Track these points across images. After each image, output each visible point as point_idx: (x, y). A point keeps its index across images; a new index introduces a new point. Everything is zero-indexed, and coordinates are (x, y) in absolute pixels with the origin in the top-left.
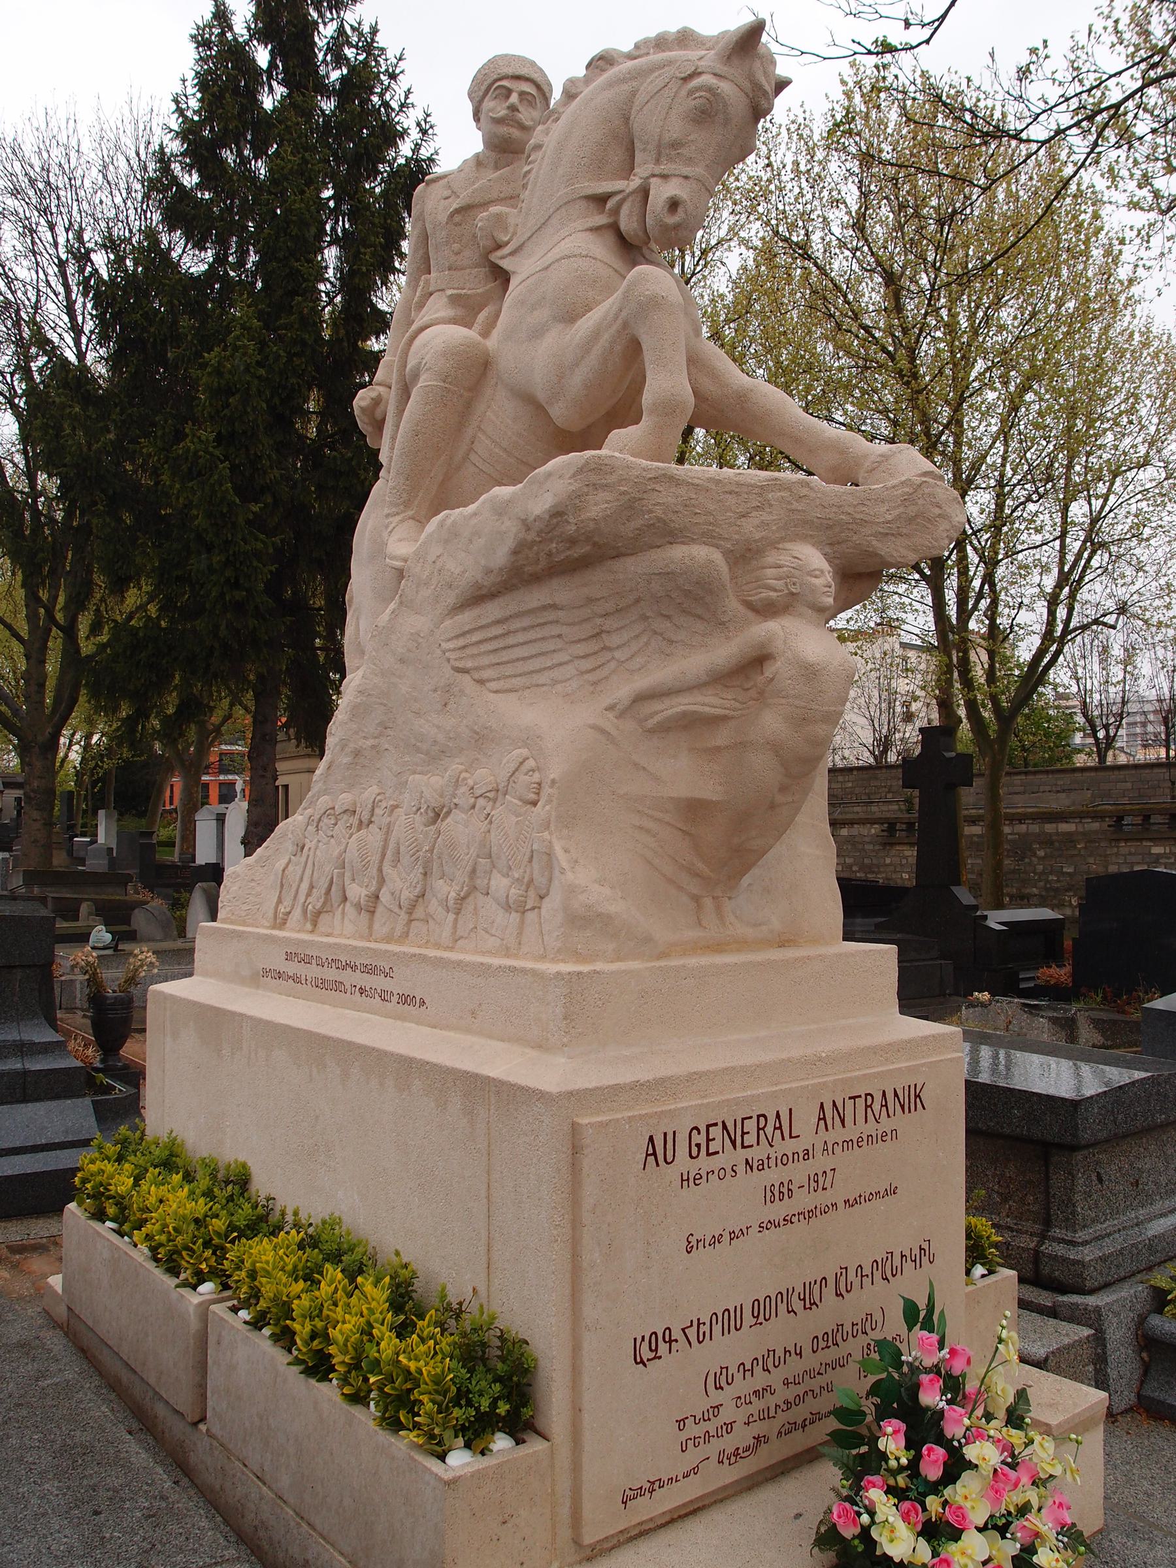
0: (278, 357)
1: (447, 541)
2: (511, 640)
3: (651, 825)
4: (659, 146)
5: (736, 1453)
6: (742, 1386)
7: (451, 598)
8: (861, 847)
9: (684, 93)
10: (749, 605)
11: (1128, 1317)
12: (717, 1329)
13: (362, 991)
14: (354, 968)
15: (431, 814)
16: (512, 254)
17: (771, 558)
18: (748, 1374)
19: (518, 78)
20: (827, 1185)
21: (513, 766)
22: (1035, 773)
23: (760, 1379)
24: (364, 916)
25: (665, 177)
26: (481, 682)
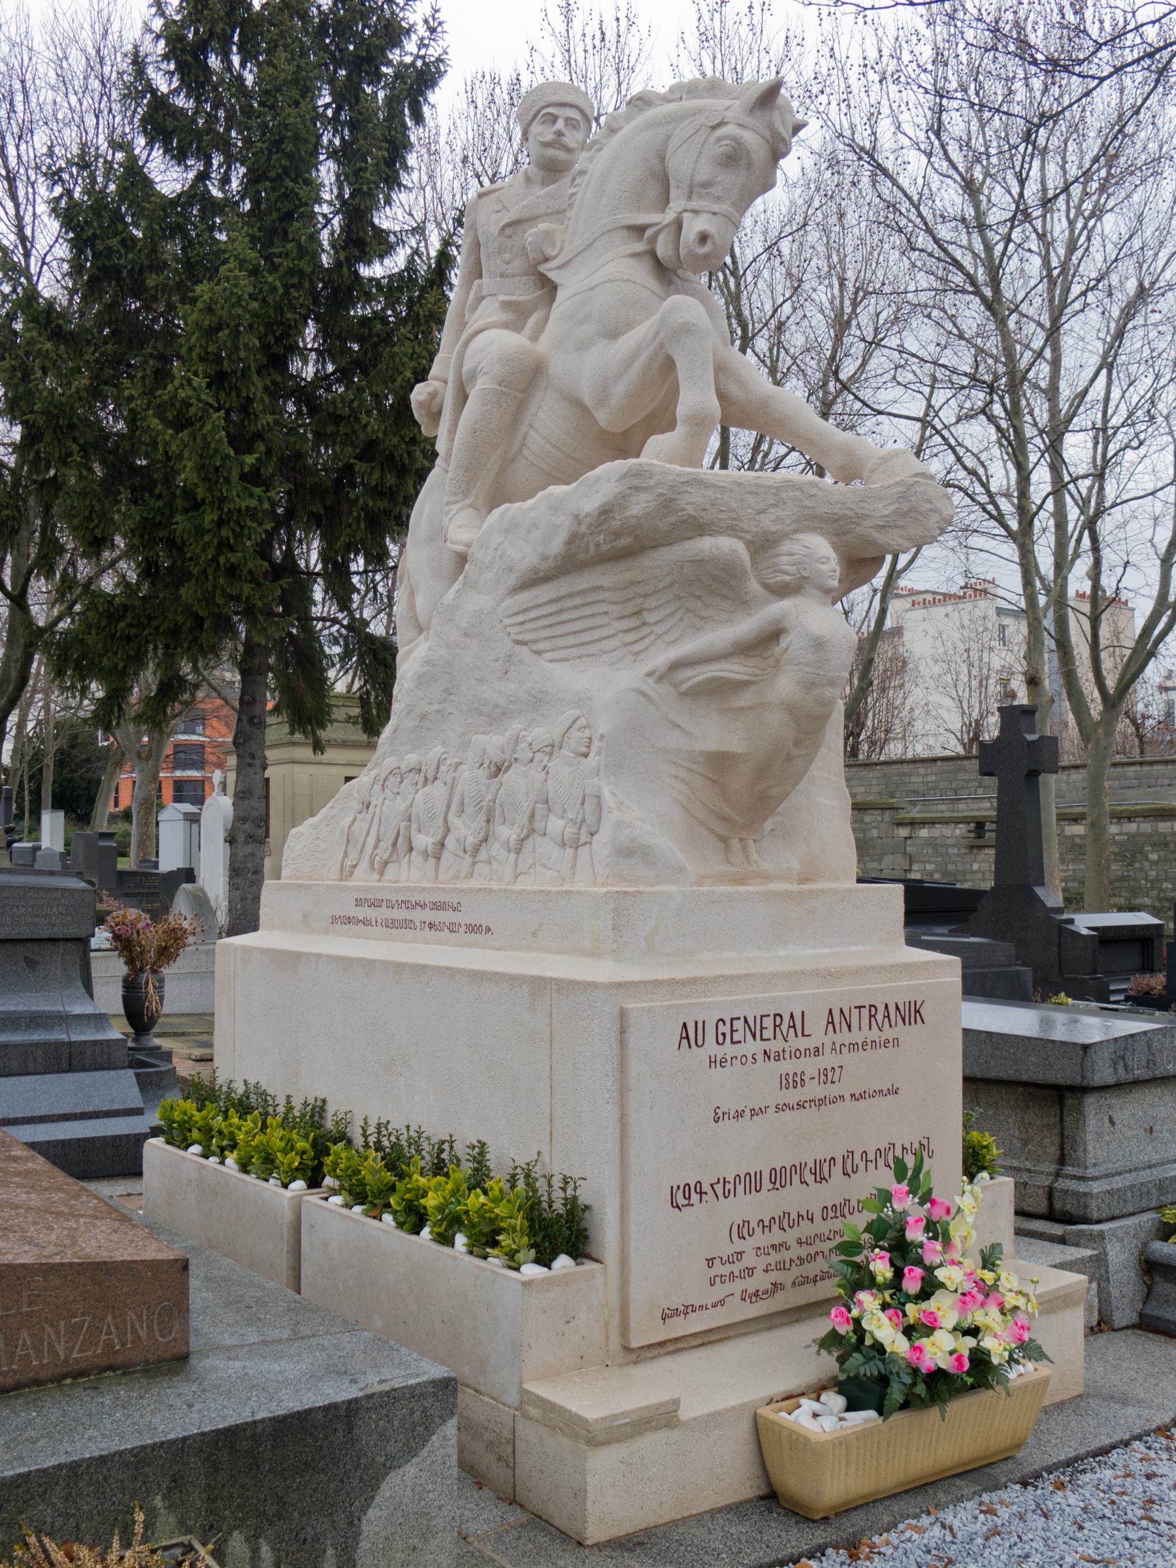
0: (275, 288)
1: (507, 531)
2: (564, 617)
4: (691, 186)
5: (756, 1294)
6: (762, 1239)
7: (512, 580)
8: (943, 850)
9: (712, 139)
11: (1132, 1244)
12: (740, 1188)
13: (431, 926)
14: (423, 906)
15: (493, 768)
16: (559, 268)
17: (786, 546)
19: (563, 105)
20: (836, 1079)
21: (567, 724)
22: (1152, 763)
23: (776, 1236)
24: (431, 862)
25: (695, 212)
26: (538, 653)
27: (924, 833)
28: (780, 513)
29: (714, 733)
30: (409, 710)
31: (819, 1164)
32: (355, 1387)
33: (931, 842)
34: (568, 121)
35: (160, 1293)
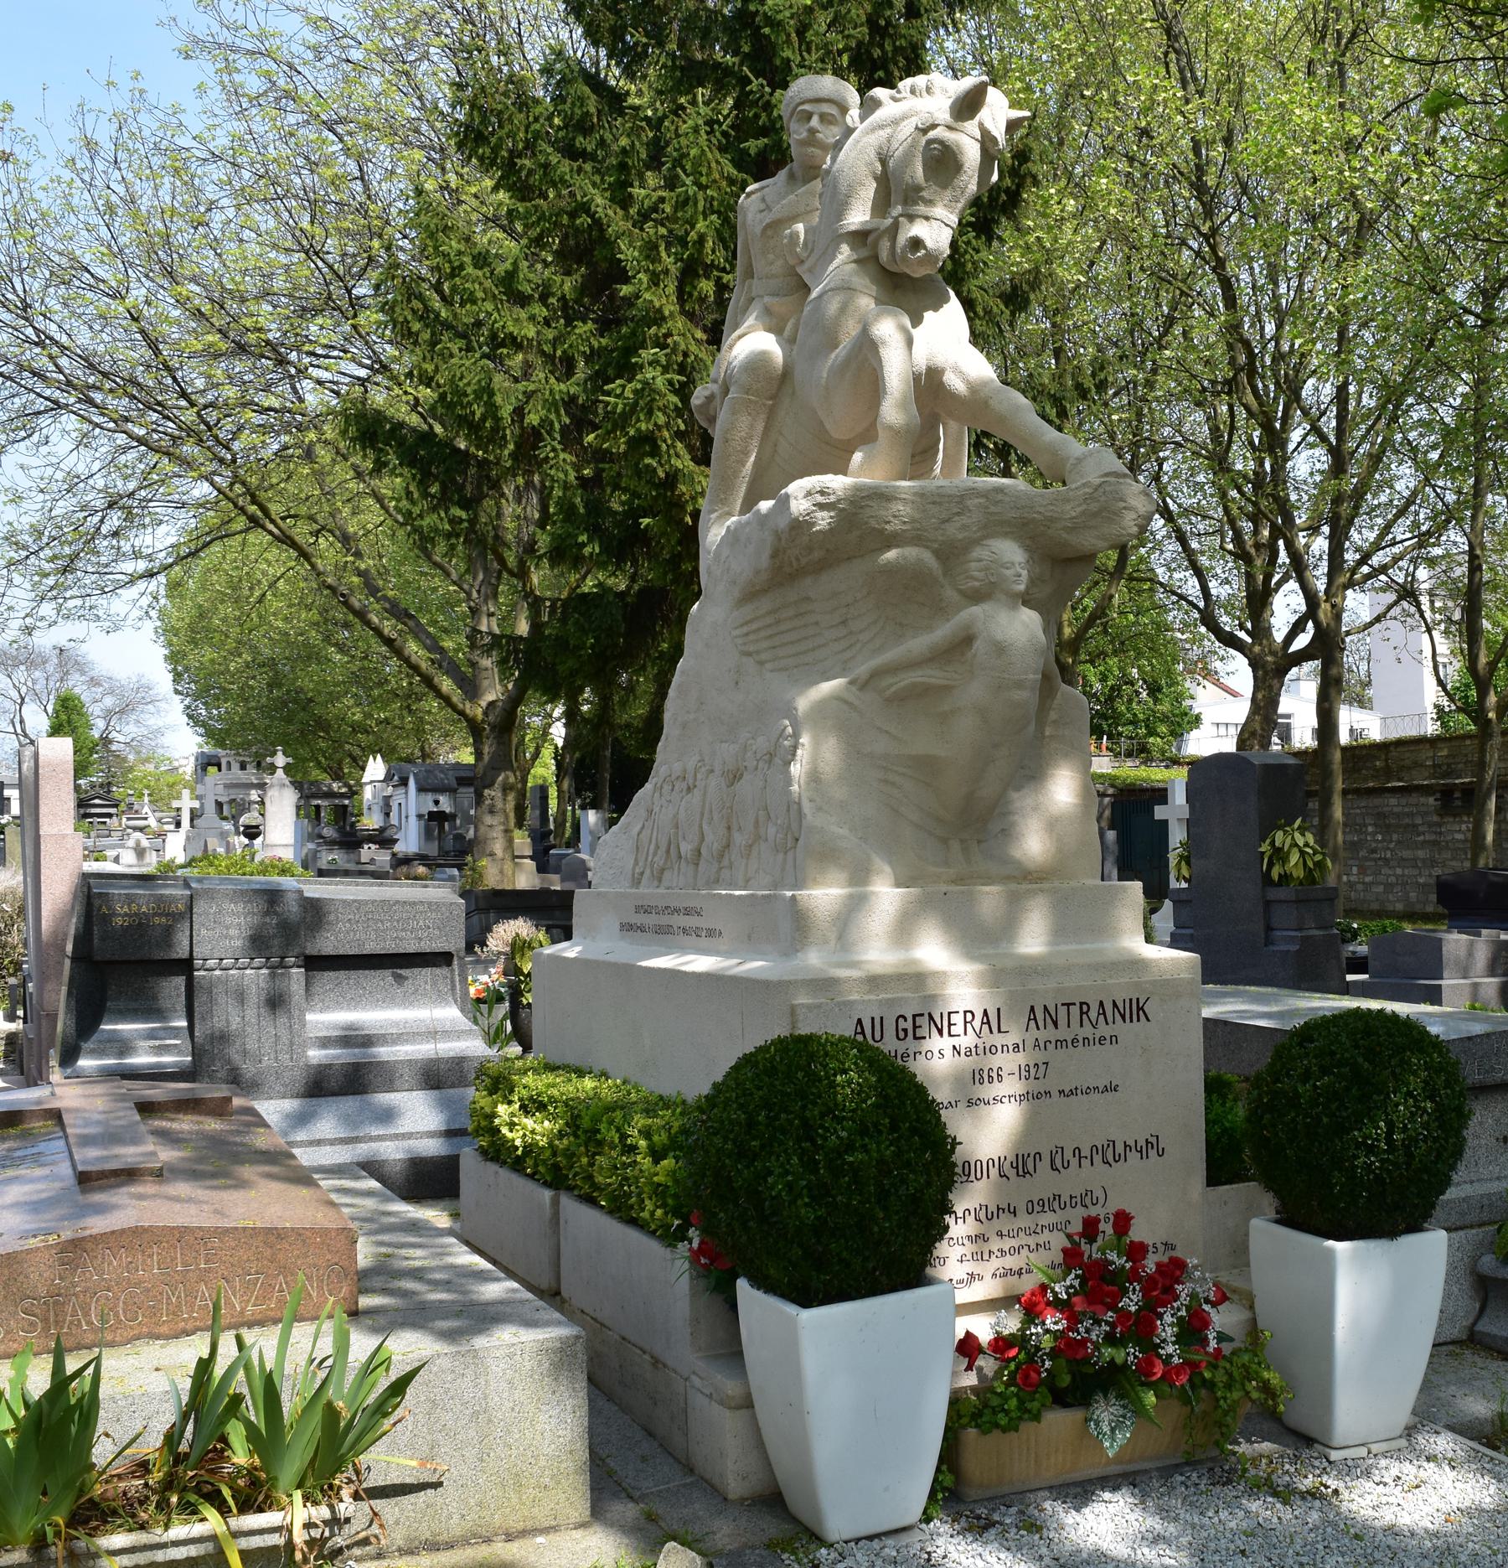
2: (783, 627)
10: (962, 593)
17: (977, 552)
24: (692, 867)
28: (964, 520)
35: (329, 1257)
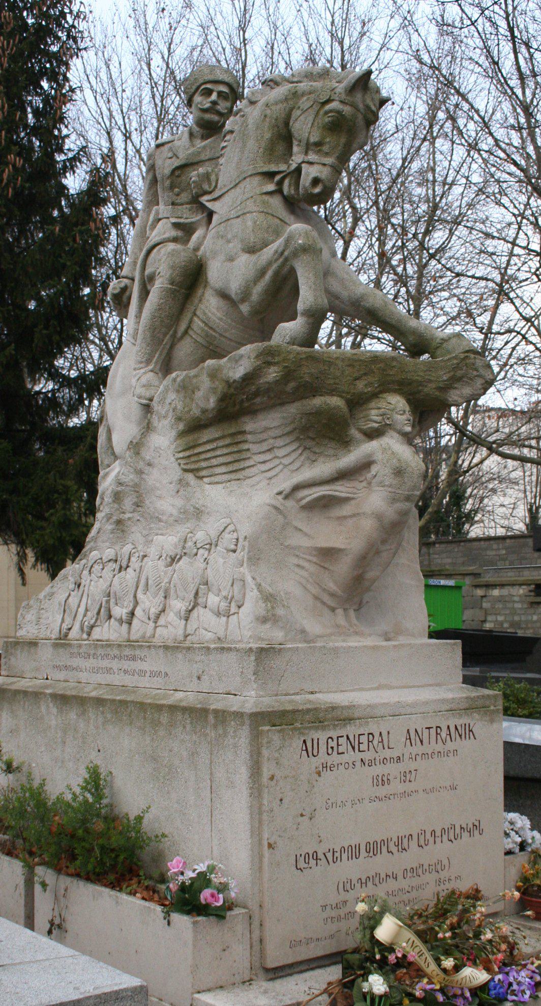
2: (218, 452)
3: (306, 564)
13: (126, 672)
15: (169, 560)
18: (364, 885)
20: (412, 779)
25: (311, 163)
27: (496, 592)
29: (327, 533)
30: (109, 517)
31: (400, 840)
32: (77, 992)
33: (501, 599)
34: (220, 94)
